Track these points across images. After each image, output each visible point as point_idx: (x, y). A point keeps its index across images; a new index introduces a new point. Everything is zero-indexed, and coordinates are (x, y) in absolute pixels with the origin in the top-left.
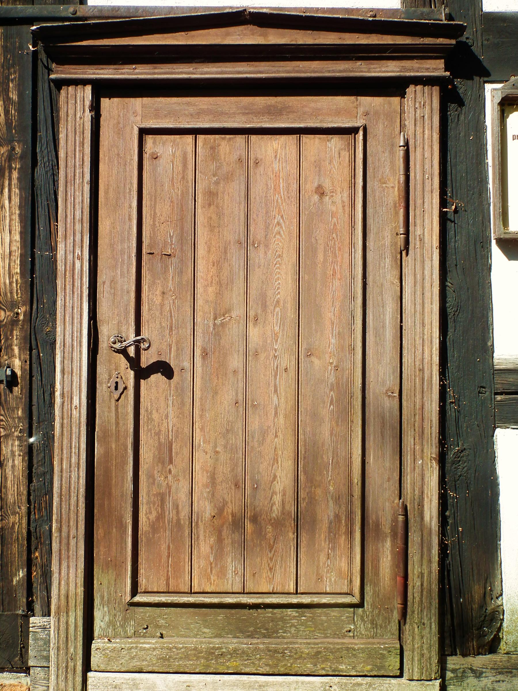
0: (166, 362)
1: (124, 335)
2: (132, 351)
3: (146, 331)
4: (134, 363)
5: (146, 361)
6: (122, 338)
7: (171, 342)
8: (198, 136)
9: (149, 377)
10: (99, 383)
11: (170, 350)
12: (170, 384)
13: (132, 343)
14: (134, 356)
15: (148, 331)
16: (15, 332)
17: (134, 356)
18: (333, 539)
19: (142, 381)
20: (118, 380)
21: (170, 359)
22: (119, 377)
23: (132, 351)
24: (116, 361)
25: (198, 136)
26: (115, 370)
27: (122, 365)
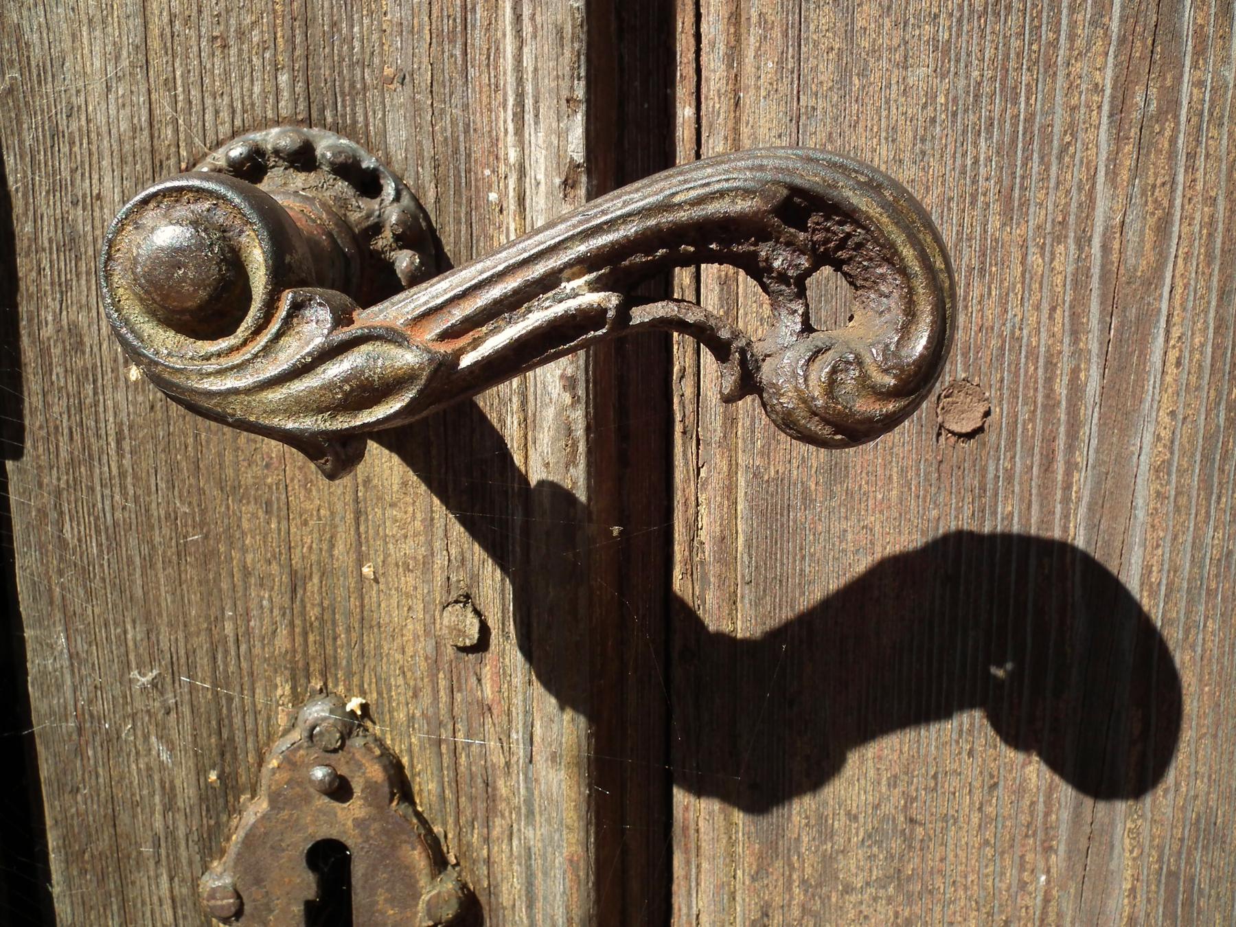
0: (1053, 557)
1: (397, 137)
2: (545, 426)
3: (762, 65)
4: (593, 590)
5: (762, 531)
6: (368, 184)
7: (1139, 232)
8: (703, 266)
9: (819, 770)
10: (72, 858)
11: (1124, 363)
12: (1089, 852)
13: (579, 295)
14: (576, 480)
15: (795, 72)
16: (1180, 637)
17: (576, 480)
18: (330, 235)
19: (704, 824)
20: (345, 821)
21: (1111, 495)
22: (368, 772)
23: (545, 426)
24: (306, 540)
25: (703, 266)
26: (298, 675)
27: (389, 609)
